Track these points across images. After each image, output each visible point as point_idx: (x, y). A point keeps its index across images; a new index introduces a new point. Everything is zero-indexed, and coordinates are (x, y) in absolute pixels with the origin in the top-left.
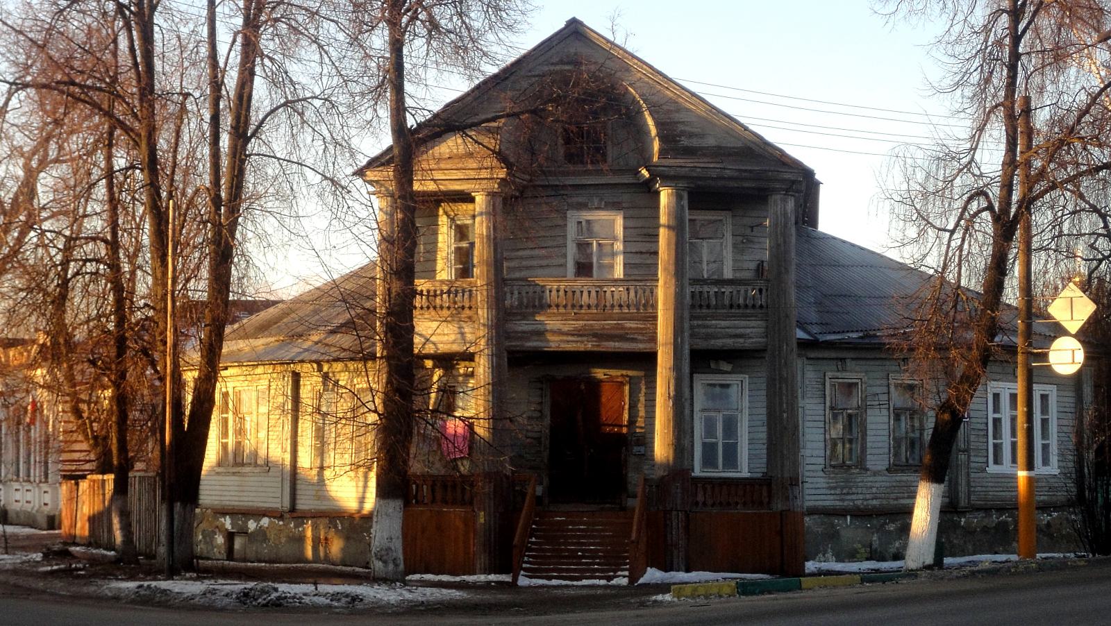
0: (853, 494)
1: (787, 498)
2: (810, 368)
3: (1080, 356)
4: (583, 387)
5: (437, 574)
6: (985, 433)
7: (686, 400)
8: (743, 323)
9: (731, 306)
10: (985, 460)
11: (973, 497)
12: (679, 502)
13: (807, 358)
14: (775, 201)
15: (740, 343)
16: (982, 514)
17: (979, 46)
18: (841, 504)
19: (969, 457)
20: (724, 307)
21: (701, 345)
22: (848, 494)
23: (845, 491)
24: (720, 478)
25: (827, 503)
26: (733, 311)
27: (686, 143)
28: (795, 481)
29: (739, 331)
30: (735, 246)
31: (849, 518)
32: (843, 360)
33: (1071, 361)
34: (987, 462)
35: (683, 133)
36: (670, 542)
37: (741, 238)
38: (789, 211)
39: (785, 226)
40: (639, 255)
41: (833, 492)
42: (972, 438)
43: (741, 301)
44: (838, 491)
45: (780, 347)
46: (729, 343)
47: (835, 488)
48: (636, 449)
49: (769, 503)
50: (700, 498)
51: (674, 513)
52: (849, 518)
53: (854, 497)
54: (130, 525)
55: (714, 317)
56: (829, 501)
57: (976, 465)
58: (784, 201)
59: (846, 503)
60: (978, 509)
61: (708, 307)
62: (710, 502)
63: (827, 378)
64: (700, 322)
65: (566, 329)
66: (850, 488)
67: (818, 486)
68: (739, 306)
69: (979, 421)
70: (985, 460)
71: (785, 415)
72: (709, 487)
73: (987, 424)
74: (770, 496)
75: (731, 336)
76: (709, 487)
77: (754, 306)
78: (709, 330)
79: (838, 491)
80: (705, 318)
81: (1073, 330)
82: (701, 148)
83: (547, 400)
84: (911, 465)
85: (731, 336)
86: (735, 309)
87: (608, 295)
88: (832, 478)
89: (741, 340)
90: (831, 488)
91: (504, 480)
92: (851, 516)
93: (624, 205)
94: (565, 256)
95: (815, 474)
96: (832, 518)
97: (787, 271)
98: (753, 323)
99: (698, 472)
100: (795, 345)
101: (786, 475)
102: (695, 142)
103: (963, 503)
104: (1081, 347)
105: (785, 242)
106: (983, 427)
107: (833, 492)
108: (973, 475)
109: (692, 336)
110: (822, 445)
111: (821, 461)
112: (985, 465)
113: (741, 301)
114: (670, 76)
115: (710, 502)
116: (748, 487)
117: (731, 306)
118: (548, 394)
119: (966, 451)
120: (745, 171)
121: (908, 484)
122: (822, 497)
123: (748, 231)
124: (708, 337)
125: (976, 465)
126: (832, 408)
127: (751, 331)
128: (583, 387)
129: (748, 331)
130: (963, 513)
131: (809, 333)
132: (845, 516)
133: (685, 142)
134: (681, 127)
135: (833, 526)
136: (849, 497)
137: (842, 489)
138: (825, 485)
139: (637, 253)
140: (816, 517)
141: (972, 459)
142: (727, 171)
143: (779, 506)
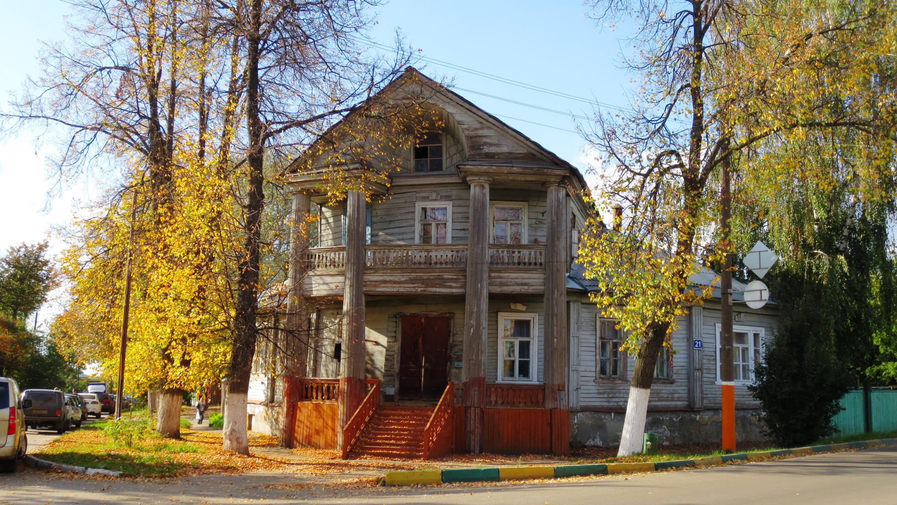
0: (617, 397)
1: (556, 400)
2: (584, 310)
3: (766, 295)
4: (423, 321)
5: (800, 446)
6: (714, 358)
7: (484, 328)
8: (527, 275)
9: (519, 264)
10: (714, 376)
11: (704, 401)
12: (476, 401)
13: (582, 303)
14: (552, 191)
15: (530, 290)
16: (712, 413)
17: (664, 47)
18: (607, 404)
19: (702, 374)
20: (514, 264)
21: (497, 289)
22: (613, 397)
23: (610, 396)
24: (527, 385)
25: (598, 404)
26: (520, 267)
27: (487, 151)
28: (561, 388)
29: (525, 281)
30: (530, 226)
31: (613, 414)
32: (740, 313)
33: (759, 299)
34: (716, 378)
35: (486, 144)
36: (469, 429)
37: (535, 221)
38: (561, 198)
39: (558, 207)
40: (462, 232)
41: (601, 396)
42: (705, 361)
43: (527, 260)
44: (606, 396)
45: (553, 293)
46: (517, 289)
47: (603, 393)
48: (456, 364)
49: (543, 403)
50: (493, 399)
51: (473, 409)
52: (613, 414)
53: (617, 400)
54: (721, 432)
55: (506, 271)
56: (598, 402)
57: (707, 379)
58: (558, 192)
59: (611, 404)
60: (708, 409)
61: (503, 263)
62: (500, 401)
63: (598, 318)
64: (496, 274)
65: (403, 279)
66: (615, 393)
67: (591, 391)
68: (525, 264)
69: (710, 350)
70: (714, 376)
71: (555, 340)
72: (499, 390)
73: (715, 352)
74: (544, 399)
75: (518, 285)
76: (499, 390)
77: (535, 264)
78: (503, 280)
79: (606, 396)
80: (499, 271)
81: (761, 276)
82: (498, 154)
83: (400, 330)
84: (660, 379)
85: (522, 284)
86: (522, 265)
87: (433, 257)
88: (602, 386)
89: (526, 287)
90: (600, 393)
91: (358, 383)
92: (615, 413)
93: (453, 198)
94: (414, 232)
95: (588, 384)
96: (600, 414)
97: (559, 238)
98: (534, 276)
99: (500, 380)
100: (564, 292)
101: (556, 383)
102: (493, 150)
103: (698, 405)
104: (766, 288)
105: (557, 219)
106: (714, 354)
107: (601, 396)
108: (704, 386)
109: (490, 284)
110: (594, 363)
111: (593, 374)
112: (714, 380)
113: (527, 260)
114: (533, 139)
115: (500, 401)
116: (511, 391)
117: (519, 264)
118: (400, 326)
119: (700, 369)
120: (527, 168)
121: (658, 391)
122: (595, 400)
123: (540, 216)
124: (501, 285)
125: (707, 379)
126: (601, 338)
127: (534, 281)
128: (423, 321)
129: (531, 281)
130: (698, 412)
131: (581, 285)
132: (610, 413)
133: (486, 150)
134: (485, 140)
135: (601, 419)
136: (613, 400)
137: (608, 394)
138: (596, 391)
139: (461, 230)
140: (588, 413)
141: (705, 375)
142: (514, 168)
143: (549, 405)
